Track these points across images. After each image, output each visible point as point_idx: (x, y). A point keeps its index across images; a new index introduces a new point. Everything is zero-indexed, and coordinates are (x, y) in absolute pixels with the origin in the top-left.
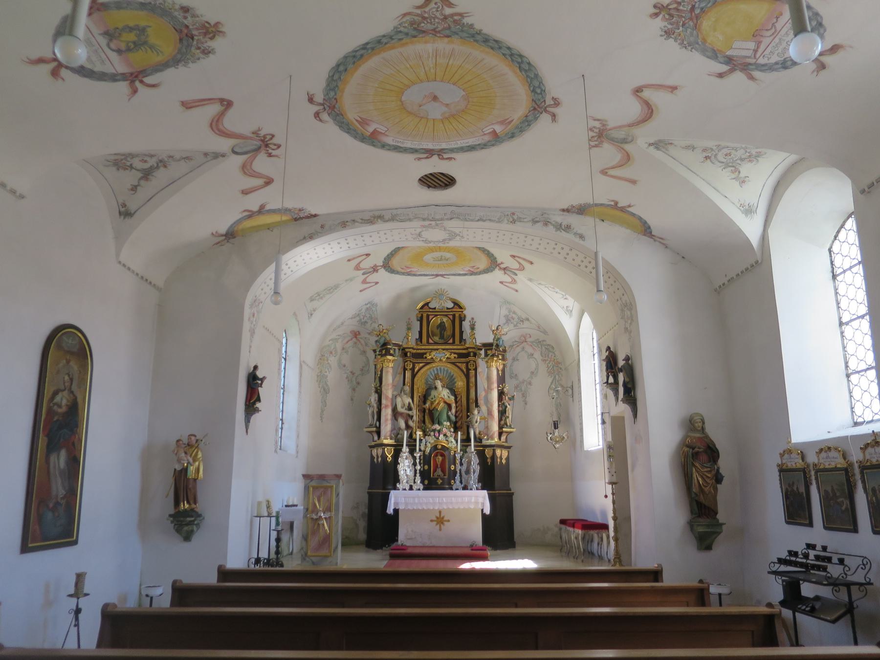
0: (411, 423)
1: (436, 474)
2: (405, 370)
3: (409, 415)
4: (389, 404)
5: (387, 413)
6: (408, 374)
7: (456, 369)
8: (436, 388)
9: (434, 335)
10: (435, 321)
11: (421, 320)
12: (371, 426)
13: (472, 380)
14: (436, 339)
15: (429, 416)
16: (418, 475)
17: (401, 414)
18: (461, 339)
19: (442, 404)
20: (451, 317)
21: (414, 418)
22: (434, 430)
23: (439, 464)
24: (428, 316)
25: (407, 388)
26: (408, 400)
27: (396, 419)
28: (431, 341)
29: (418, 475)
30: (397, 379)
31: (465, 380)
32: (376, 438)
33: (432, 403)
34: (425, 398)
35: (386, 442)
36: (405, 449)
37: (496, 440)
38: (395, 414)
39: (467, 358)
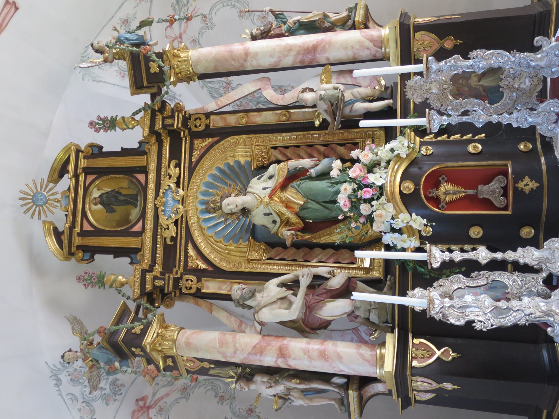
0: (337, 282)
1: (499, 201)
2: (199, 295)
3: (311, 287)
4: (276, 343)
5: (303, 352)
6: (212, 286)
7: (206, 162)
8: (245, 211)
9: (126, 220)
10: (95, 213)
11: (91, 252)
12: (343, 403)
13: (232, 120)
14: (135, 213)
15: (316, 233)
16: (510, 255)
17: (309, 308)
18: (139, 152)
19: (290, 194)
20: (90, 178)
21: (323, 270)
23: (462, 192)
24: (83, 234)
25: (237, 289)
26: (272, 288)
27: (325, 325)
28: (138, 227)
29: (510, 255)
30: (222, 316)
31: (231, 139)
32: (379, 388)
33: (287, 223)
34: (274, 244)
35: (390, 364)
36: (416, 300)
37: (385, 32)
38: (308, 326)
39: (175, 133)
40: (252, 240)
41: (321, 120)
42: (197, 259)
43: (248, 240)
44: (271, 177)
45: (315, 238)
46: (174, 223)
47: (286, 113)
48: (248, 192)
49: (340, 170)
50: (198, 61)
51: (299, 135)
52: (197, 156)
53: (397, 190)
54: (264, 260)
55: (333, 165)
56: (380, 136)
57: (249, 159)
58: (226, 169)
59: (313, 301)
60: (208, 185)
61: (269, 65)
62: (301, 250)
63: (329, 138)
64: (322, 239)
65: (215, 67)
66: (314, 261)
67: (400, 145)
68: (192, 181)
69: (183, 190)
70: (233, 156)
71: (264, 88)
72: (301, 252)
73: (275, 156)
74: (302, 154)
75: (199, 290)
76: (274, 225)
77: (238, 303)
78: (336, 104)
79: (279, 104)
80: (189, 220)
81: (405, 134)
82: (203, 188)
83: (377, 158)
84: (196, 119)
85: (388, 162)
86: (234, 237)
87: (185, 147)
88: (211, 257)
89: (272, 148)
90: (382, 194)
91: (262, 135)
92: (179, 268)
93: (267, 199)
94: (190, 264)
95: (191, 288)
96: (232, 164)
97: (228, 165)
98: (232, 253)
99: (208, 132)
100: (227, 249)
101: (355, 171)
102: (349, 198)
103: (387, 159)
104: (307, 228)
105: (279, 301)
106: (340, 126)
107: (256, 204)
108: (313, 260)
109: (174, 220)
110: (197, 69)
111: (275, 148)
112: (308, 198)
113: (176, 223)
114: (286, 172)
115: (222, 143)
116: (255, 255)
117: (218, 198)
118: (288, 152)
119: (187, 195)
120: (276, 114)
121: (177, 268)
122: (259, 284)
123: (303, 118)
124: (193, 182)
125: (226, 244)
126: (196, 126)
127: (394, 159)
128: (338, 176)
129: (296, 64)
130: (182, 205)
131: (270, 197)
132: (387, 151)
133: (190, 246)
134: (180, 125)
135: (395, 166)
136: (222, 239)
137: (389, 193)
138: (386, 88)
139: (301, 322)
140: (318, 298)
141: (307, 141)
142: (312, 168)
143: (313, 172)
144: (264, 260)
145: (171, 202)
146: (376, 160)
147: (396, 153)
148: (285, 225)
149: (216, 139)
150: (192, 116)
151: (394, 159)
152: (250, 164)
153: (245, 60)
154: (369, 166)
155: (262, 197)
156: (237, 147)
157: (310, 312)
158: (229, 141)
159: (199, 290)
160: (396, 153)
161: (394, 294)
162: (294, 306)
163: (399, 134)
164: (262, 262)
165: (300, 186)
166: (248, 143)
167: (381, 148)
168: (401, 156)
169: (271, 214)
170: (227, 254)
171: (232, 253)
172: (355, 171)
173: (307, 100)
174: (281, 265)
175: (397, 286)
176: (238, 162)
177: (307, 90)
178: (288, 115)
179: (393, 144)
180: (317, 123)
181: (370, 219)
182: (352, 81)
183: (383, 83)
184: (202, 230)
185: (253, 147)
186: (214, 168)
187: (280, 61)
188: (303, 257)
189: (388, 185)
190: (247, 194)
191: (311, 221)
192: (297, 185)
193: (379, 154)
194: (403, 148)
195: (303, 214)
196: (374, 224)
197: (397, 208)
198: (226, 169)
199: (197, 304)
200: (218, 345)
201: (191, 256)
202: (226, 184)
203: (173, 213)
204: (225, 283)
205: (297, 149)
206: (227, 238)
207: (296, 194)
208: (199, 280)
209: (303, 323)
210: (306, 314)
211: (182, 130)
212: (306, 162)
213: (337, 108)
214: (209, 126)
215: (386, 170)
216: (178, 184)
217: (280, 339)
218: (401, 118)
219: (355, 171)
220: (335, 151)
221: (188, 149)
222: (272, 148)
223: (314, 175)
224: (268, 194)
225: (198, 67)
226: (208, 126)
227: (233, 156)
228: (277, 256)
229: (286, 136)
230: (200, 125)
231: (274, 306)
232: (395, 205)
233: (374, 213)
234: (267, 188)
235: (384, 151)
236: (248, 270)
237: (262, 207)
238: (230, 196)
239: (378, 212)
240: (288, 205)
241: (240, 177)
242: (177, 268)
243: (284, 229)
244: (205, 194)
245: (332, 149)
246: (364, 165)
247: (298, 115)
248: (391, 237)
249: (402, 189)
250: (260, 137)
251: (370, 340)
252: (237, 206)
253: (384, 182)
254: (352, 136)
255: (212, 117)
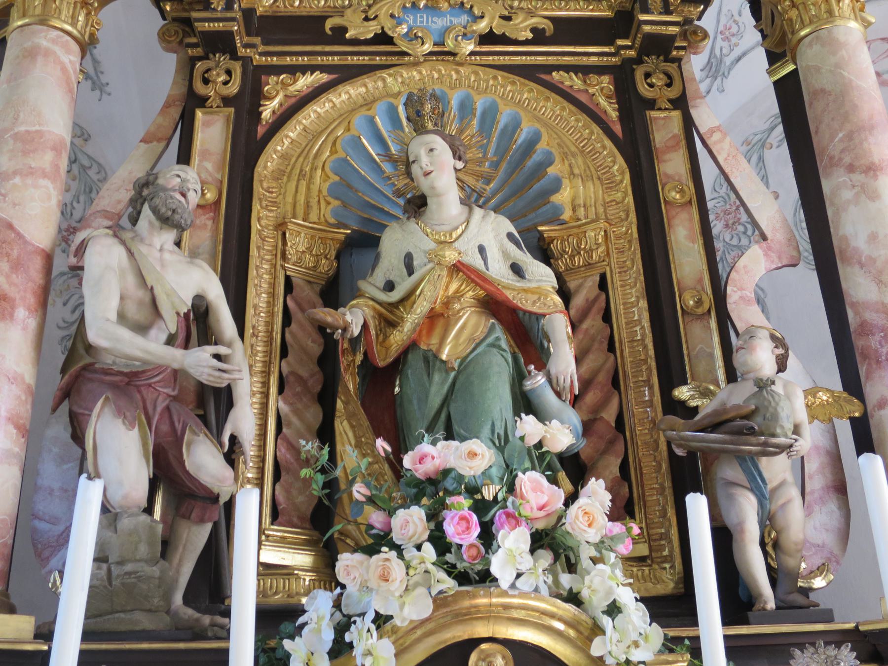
0: (204, 460)
2: (190, 103)
6: (212, 133)
7: (552, 107)
8: (418, 205)
13: (672, 166)
17: (128, 385)
21: (244, 421)
22: (433, 490)
26: (193, 279)
40: (342, 237)
41: (693, 404)
42: (286, 96)
43: (341, 225)
44: (517, 270)
45: (346, 403)
46: (384, 32)
47: (706, 306)
48: (471, 210)
49: (539, 445)
50: (832, 45)
51: (645, 347)
52: (567, 83)
53: (481, 630)
54: (283, 267)
55: (554, 422)
56: (659, 581)
57: (567, 215)
58: (536, 157)
59: (149, 395)
60: (490, 115)
61: (845, 238)
62: (317, 369)
63: (640, 431)
64: (345, 423)
65: (823, 91)
66: (281, 405)
67: (634, 636)
68: (500, 75)
69: (472, 53)
70: (572, 173)
71: (769, 248)
72: (309, 371)
73: (580, 286)
74: (591, 362)
75: (202, 101)
76: (381, 284)
77: (146, 184)
78: (748, 430)
79: (729, 289)
80: (391, 71)
81: (671, 651)
82: (480, 103)
83: (585, 563)
84: (669, 76)
85: (574, 598)
86: (350, 186)
87: (592, 53)
88: (292, 132)
89: (603, 277)
90: (463, 578)
91: (636, 245)
92: (261, 54)
93: (451, 256)
94: (273, 79)
95: (206, 81)
96: (551, 170)
97: (548, 161)
98: (303, 183)
99: (634, 109)
100: (314, 169)
101: (537, 492)
102: (446, 472)
103: (585, 593)
104: (380, 380)
105: (147, 298)
106: (680, 452)
107: (438, 228)
108: (286, 401)
109: (390, 33)
110: (810, 45)
111: (603, 284)
112: (459, 372)
113: (383, 38)
114: (535, 309)
115: (608, 143)
116: (298, 243)
117: (452, 129)
118: (593, 323)
119: (461, 64)
120: (700, 280)
121: (261, 49)
122: (213, 256)
123: (693, 353)
124: (495, 78)
125: (327, 168)
126: (648, 75)
127: (584, 617)
128: (522, 438)
129: (857, 313)
130: (431, 53)
131: (458, 268)
132: (610, 591)
133: (321, 77)
134: (647, 28)
135: (560, 619)
136: (341, 154)
137: (467, 603)
138: (806, 592)
139: (88, 360)
140: (159, 409)
141: (629, 371)
142: (550, 380)
143: (537, 381)
144: (283, 267)
145: (439, 23)
146: (577, 556)
147: (606, 622)
148: (380, 315)
149: (618, 129)
150: (675, 65)
151: (584, 617)
152: (555, 219)
153: (851, 169)
154: (558, 534)
155: (456, 244)
156: (597, 182)
157: (114, 386)
158: (614, 162)
159: (202, 101)
160: (606, 622)
161: (87, 635)
162: (126, 334)
163: (673, 633)
164: (279, 262)
165: (495, 350)
166: (611, 211)
167: (619, 573)
168: (597, 641)
169: (410, 272)
170: (301, 171)
171: (303, 183)
172: (537, 489)
173: (751, 349)
174: (271, 314)
175: (181, 646)
176: (556, 186)
177: (780, 351)
178: (700, 311)
179: (636, 615)
180: (683, 393)
181: (379, 542)
182: (812, 492)
183: (819, 583)
184: (366, 105)
185: (602, 224)
186: (537, 126)
187: (862, 266)
188: (292, 373)
189: (494, 600)
190: (466, 209)
191: (397, 390)
192: (498, 339)
193: (600, 566)
194: (623, 646)
195: (415, 362)
196: (359, 557)
197: (419, 632)
198: (536, 157)
199: (167, 105)
200: (22, 129)
201: (295, 81)
202: (496, 165)
203: (410, 29)
204: (220, 168)
205: (605, 345)
206: (343, 167)
207: (471, 339)
208: (227, 101)
209: (85, 368)
210: (107, 372)
211: (633, 43)
212: (564, 361)
213: (739, 432)
214: (653, 109)
215: (544, 591)
216: (488, 38)
217: (31, 300)
218: (726, 638)
219: (537, 489)
220: (605, 452)
221: (585, 60)
222: (603, 277)
223: (528, 384)
224: (466, 260)
225: (816, 48)
226: (651, 104)
227: (572, 173)
228: (299, 304)
229: (641, 312)
230: (651, 85)
231: (131, 280)
232: (430, 626)
233: (394, 554)
234: (485, 259)
235: (607, 581)
236: (255, 226)
237: (430, 245)
238: (458, 156)
239: (397, 567)
240: (437, 319)
241: (518, 190)
242: (261, 49)
243: (369, 313)
244: (466, 108)
245: (611, 442)
246: (560, 518)
247: (701, 341)
248: (320, 618)
249: (484, 646)
250: (630, 242)
251: (51, 572)
252: (427, 174)
253: (504, 584)
254: (652, 497)
255: (676, 115)
